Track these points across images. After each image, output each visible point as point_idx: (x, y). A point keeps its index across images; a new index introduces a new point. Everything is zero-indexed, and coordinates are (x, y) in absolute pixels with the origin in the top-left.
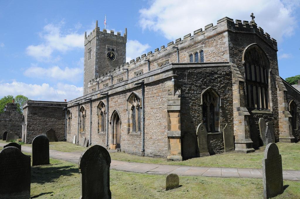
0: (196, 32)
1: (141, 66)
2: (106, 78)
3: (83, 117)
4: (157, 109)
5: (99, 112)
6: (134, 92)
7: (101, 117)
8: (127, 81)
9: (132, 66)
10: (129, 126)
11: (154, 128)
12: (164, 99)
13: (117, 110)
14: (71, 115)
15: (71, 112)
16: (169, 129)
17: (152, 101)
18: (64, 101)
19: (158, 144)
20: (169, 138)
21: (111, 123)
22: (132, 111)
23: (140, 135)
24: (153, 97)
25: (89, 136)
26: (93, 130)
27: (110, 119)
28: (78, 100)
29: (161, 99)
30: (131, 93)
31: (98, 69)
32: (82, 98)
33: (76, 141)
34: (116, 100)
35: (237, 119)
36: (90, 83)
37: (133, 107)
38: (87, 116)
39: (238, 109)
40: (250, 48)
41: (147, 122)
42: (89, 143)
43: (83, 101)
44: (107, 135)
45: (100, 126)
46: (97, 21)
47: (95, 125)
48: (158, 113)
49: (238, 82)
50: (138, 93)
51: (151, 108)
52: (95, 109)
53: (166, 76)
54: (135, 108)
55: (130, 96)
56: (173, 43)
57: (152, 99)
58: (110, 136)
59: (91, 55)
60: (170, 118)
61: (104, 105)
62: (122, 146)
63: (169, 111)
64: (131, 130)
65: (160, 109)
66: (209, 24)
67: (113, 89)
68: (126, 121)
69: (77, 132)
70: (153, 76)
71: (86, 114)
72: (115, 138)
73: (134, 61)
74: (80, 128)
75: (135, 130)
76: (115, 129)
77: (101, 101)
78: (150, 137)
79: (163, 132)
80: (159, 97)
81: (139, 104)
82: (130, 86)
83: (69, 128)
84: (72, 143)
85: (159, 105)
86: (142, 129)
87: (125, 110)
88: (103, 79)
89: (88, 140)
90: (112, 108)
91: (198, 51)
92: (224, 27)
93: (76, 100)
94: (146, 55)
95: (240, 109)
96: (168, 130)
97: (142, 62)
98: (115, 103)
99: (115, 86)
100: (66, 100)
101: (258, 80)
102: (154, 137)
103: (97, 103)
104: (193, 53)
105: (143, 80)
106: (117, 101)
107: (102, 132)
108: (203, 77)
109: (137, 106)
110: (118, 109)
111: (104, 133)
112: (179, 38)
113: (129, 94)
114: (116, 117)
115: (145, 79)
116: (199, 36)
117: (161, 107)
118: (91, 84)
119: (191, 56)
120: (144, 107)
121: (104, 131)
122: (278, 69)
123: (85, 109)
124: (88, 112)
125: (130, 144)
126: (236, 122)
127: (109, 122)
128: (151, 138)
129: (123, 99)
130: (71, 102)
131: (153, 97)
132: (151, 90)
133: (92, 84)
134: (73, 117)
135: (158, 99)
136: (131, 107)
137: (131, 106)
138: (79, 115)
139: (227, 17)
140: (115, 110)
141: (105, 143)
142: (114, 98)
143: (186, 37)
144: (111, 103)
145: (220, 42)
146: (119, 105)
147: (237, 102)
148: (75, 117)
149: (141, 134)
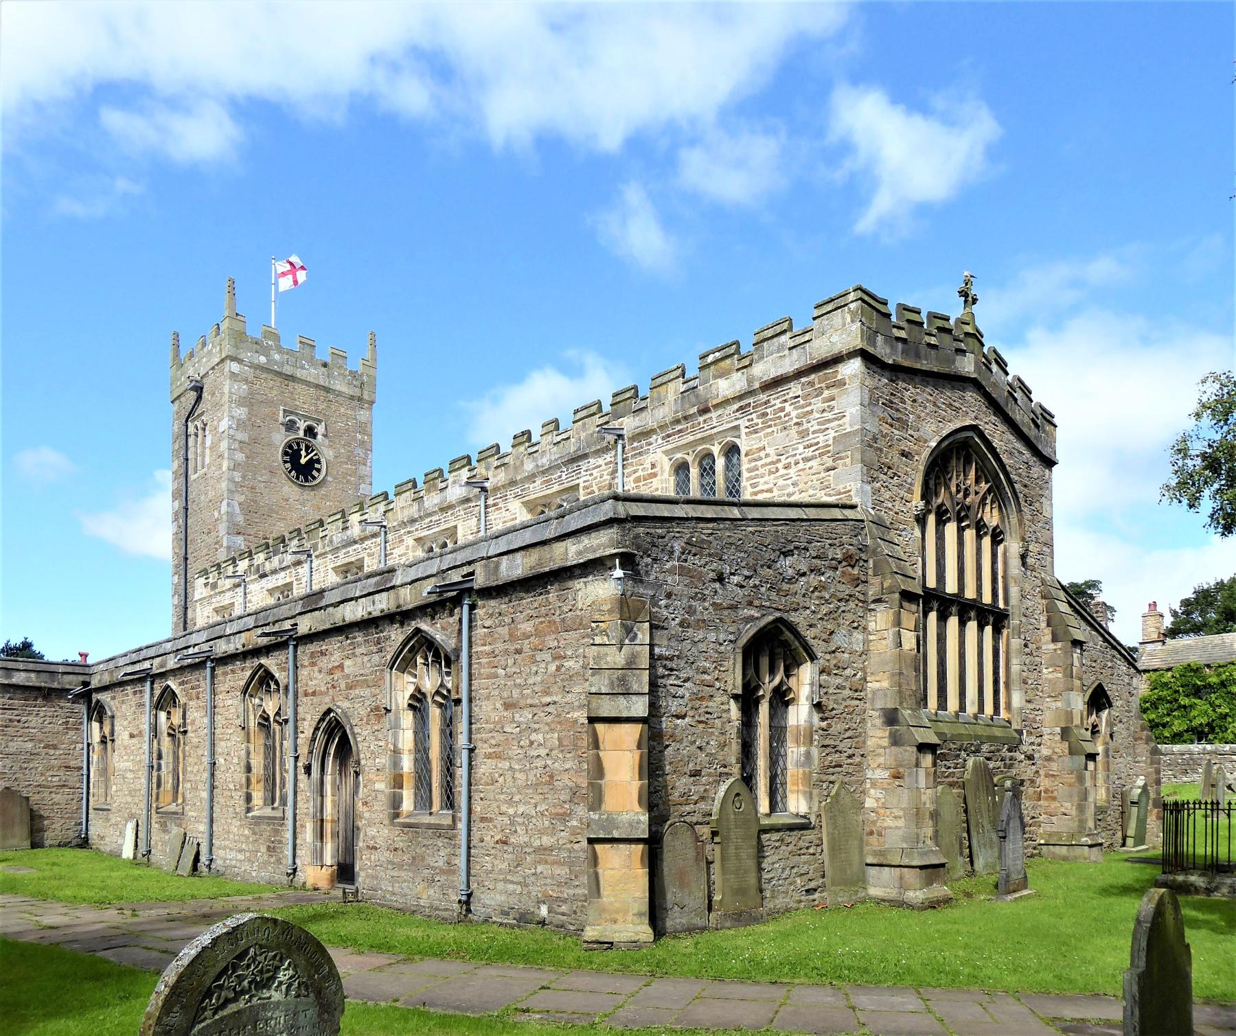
0: (710, 359)
1: (445, 509)
2: (281, 562)
3: (169, 735)
4: (535, 710)
5: (252, 717)
6: (424, 626)
7: (258, 741)
8: (388, 572)
9: (404, 506)
10: (398, 782)
11: (516, 798)
12: (569, 664)
13: (339, 711)
14: (113, 725)
15: (109, 713)
16: (596, 801)
17: (510, 670)
18: (78, 659)
19: (539, 869)
20: (591, 841)
21: (308, 769)
22: (174, 740)
23: (453, 826)
24: (518, 652)
25: (203, 827)
26: (220, 799)
27: (303, 750)
28: (143, 654)
29: (557, 663)
30: (409, 630)
31: (240, 519)
32: (169, 646)
33: (136, 846)
34: (336, 664)
35: (881, 760)
36: (202, 580)
37: (418, 702)
38: (189, 734)
39: (891, 718)
40: (946, 443)
41: (484, 768)
42: (204, 859)
43: (172, 663)
44: (289, 823)
45: (253, 780)
46: (177, 335)
47: (230, 775)
48: (536, 726)
49: (897, 595)
50: (439, 630)
51: (507, 706)
52: (230, 702)
53: (580, 553)
54: (429, 700)
55: (404, 644)
56: (600, 409)
57: (510, 662)
58: (303, 826)
59: (207, 451)
60: (601, 754)
61: (277, 683)
62: (362, 874)
63: (592, 720)
64: (407, 804)
65: (551, 709)
66: (588, 402)
67: (320, 609)
68: (383, 760)
69: (143, 805)
70: (519, 555)
71: (184, 724)
72: (329, 836)
73: (415, 486)
74: (159, 786)
75: (424, 801)
76: (329, 793)
77: (261, 666)
78: (497, 838)
79: (564, 817)
80: (547, 656)
81: (449, 685)
82: (408, 598)
83: (102, 785)
84: (116, 855)
85: (547, 693)
86: (462, 801)
87: (377, 709)
88: (268, 567)
89: (198, 844)
90: (315, 699)
91: (716, 449)
92: (844, 332)
93: (134, 657)
94: (469, 463)
95: (900, 716)
96: (592, 809)
97: (456, 492)
98: (329, 678)
99: (331, 598)
100: (84, 656)
101: (970, 594)
102: (520, 838)
103: (241, 673)
104: (690, 459)
105: (466, 570)
106: (341, 666)
107: (268, 811)
108: (748, 567)
109: (438, 693)
110: (345, 704)
111: (279, 814)
112: (596, 400)
113: (396, 635)
114: (337, 739)
115: (478, 568)
116: (724, 374)
117: (555, 698)
118: (206, 585)
119: (681, 468)
120: (296, 721)
121: (276, 805)
122: (1049, 544)
123: (182, 699)
124: (197, 717)
125: (400, 866)
126: (878, 771)
127: (300, 764)
128: (505, 843)
129: (366, 659)
130: (111, 665)
131: (518, 652)
132: (507, 620)
133: (214, 586)
134: (122, 736)
135: (543, 665)
136: (407, 695)
137: (411, 689)
138: (155, 729)
139: (860, 289)
140: (329, 711)
141: (279, 861)
142: (323, 653)
143: (659, 382)
144: (312, 678)
145: (821, 406)
146: (350, 687)
147: (885, 684)
148: (132, 736)
149: (454, 821)
